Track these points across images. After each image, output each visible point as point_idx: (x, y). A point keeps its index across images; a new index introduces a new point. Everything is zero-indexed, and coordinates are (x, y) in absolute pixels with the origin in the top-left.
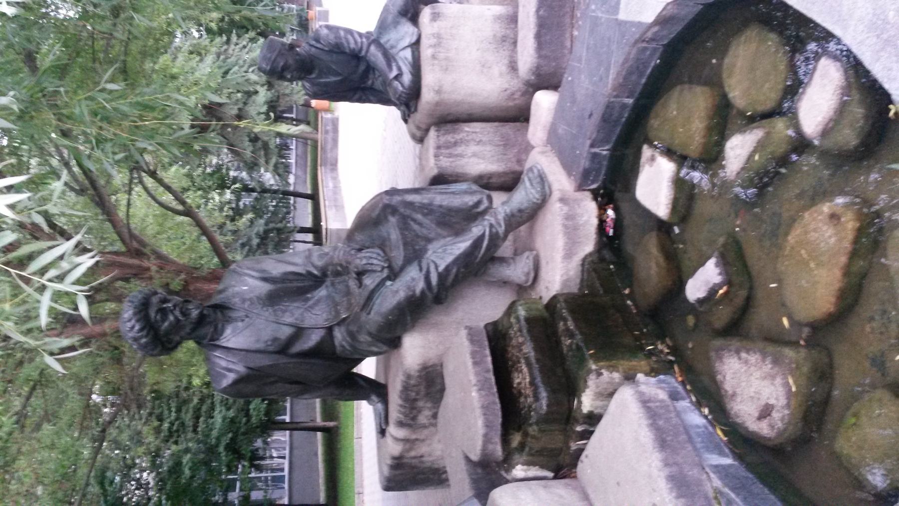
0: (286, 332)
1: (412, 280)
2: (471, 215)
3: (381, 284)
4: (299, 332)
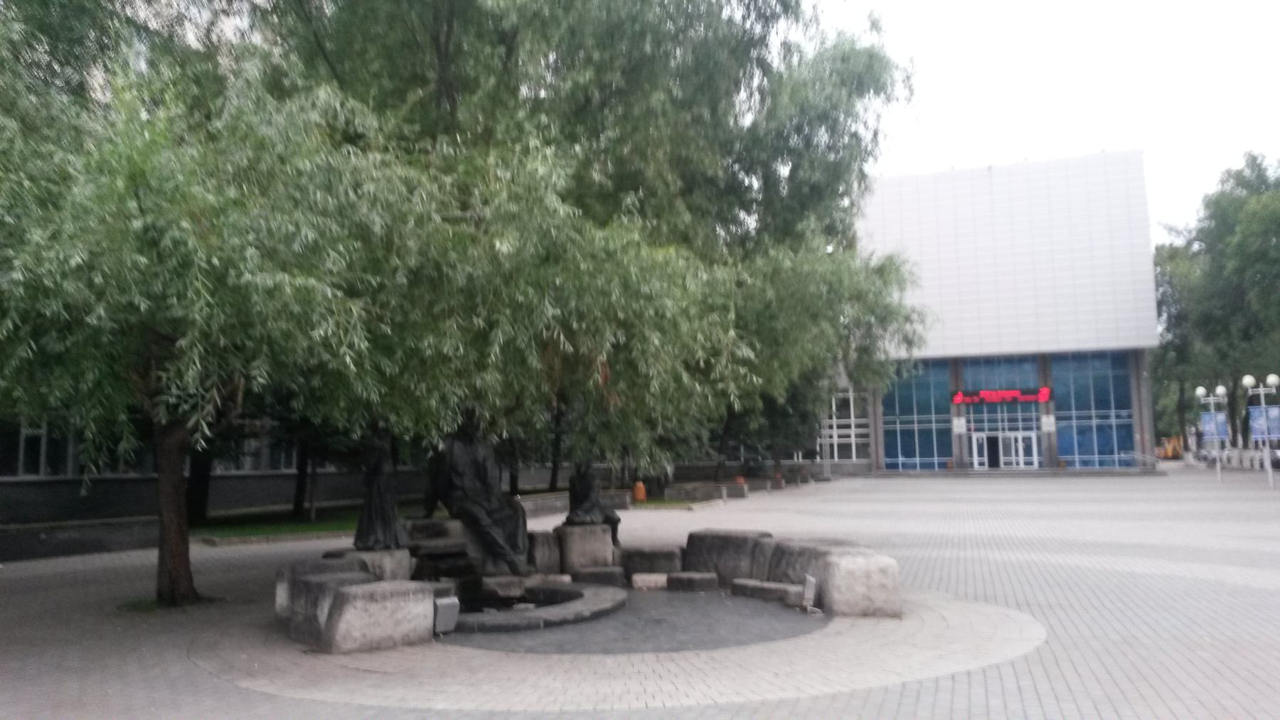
0: (460, 469)
1: (486, 520)
2: (514, 546)
3: (484, 508)
4: (460, 475)
